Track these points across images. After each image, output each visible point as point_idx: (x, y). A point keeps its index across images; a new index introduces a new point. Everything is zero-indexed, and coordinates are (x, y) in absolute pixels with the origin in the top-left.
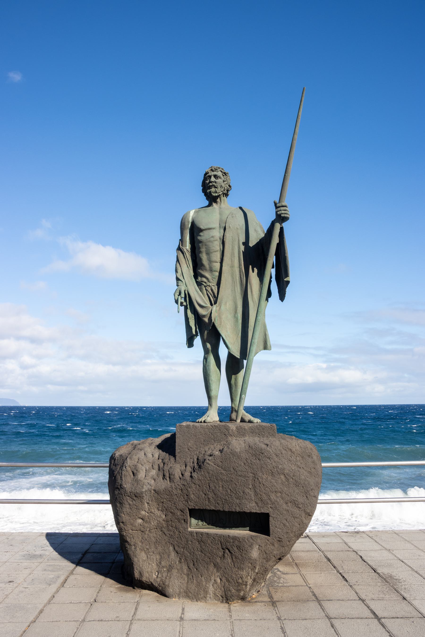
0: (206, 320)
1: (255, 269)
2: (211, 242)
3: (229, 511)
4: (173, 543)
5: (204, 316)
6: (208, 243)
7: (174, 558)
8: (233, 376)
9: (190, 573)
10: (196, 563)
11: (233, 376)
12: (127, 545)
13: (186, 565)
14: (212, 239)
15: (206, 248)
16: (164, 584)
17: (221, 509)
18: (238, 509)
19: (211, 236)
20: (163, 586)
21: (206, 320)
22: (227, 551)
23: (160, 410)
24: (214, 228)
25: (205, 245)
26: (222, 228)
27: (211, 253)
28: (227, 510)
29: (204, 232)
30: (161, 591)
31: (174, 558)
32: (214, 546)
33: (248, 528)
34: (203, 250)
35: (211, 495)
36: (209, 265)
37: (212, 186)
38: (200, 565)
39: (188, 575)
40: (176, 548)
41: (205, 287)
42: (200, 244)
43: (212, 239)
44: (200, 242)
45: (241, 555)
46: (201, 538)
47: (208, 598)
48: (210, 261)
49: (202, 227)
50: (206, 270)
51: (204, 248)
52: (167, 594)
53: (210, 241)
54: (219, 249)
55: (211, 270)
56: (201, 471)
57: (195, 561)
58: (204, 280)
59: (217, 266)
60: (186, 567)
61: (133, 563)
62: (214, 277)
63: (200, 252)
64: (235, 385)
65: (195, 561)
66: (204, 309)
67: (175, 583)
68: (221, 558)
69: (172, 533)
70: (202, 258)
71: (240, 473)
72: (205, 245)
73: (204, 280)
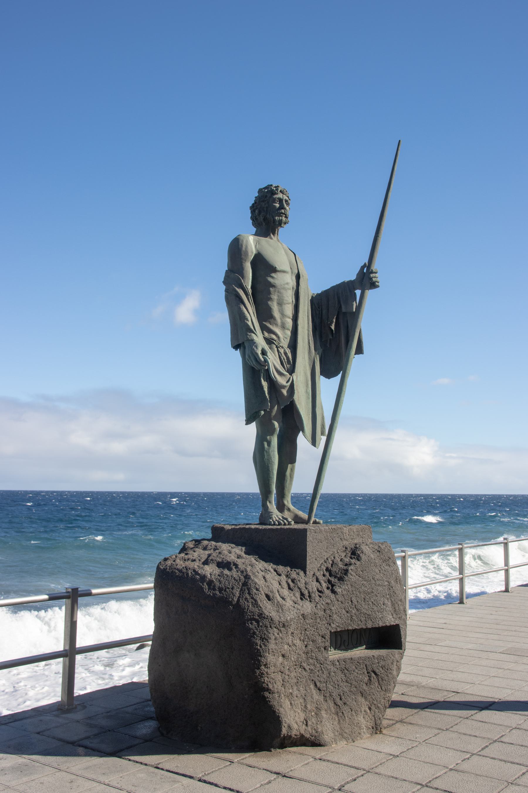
0: (285, 392)
2: (284, 289)
3: (372, 628)
4: (314, 679)
5: (284, 387)
6: (282, 291)
7: (317, 697)
8: (289, 465)
9: (338, 710)
10: (343, 697)
11: (289, 465)
12: (266, 694)
13: (332, 702)
14: (286, 286)
15: (278, 296)
16: (317, 732)
17: (364, 627)
18: (381, 624)
20: (316, 734)
21: (285, 392)
22: (373, 675)
23: (37, 505)
25: (278, 292)
27: (285, 304)
28: (369, 626)
29: (278, 273)
30: (314, 743)
31: (317, 697)
32: (359, 672)
33: (365, 646)
34: (275, 297)
35: (354, 612)
36: (281, 319)
37: (284, 214)
38: (348, 697)
39: (337, 714)
40: (318, 684)
41: (277, 347)
42: (271, 289)
43: (286, 286)
44: (273, 286)
45: (387, 676)
46: (344, 667)
47: (362, 734)
48: (283, 315)
49: (278, 268)
50: (277, 325)
52: (322, 742)
55: (283, 327)
56: (344, 584)
57: (342, 694)
58: (274, 337)
59: (289, 323)
60: (333, 705)
61: (279, 717)
62: (286, 336)
64: (291, 477)
65: (342, 694)
67: (328, 728)
68: (367, 684)
69: (312, 667)
70: (272, 307)
71: (378, 582)
72: (278, 292)
73: (274, 337)
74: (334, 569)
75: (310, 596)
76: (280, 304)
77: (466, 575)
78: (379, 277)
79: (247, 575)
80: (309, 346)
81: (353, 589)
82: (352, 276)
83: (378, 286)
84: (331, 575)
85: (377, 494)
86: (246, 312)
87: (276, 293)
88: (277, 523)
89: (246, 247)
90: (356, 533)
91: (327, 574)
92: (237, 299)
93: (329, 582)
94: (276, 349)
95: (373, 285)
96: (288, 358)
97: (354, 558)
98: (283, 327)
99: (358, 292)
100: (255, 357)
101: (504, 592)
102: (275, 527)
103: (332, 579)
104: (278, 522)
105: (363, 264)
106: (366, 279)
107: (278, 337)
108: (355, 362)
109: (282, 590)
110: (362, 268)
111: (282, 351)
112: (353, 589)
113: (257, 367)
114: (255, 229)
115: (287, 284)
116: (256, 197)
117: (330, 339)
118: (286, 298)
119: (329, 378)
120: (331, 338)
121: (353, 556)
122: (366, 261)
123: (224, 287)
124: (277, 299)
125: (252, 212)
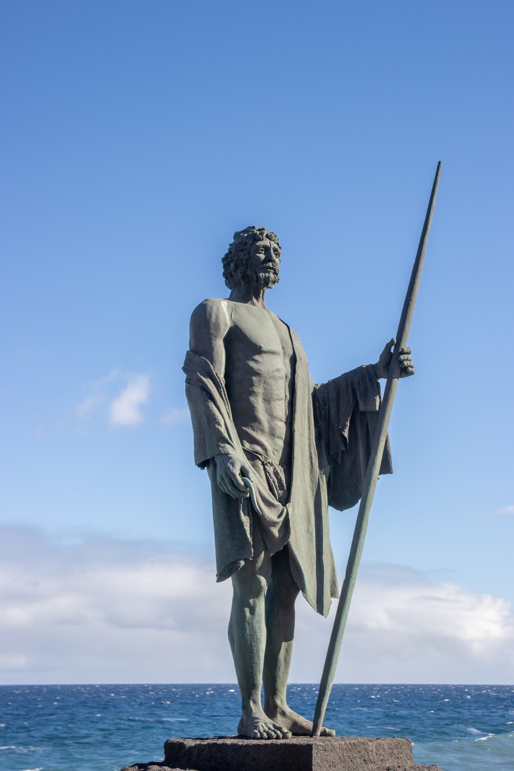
0: (275, 531)
1: (244, 441)
5: (274, 524)
6: (270, 381)
14: (277, 374)
15: (265, 389)
19: (275, 368)
21: (275, 531)
24: (273, 353)
25: (265, 382)
26: (288, 356)
27: (274, 400)
34: (259, 390)
36: (269, 422)
41: (263, 464)
42: (254, 378)
43: (277, 374)
44: (257, 374)
50: (262, 431)
51: (261, 387)
53: (273, 377)
54: (283, 395)
55: (272, 434)
58: (258, 449)
59: (281, 428)
62: (276, 448)
63: (253, 393)
64: (285, 661)
66: (273, 509)
70: (256, 405)
72: (265, 382)
73: (258, 449)
76: (267, 400)
80: (312, 462)
82: (375, 360)
83: (412, 373)
86: (217, 413)
87: (262, 384)
90: (388, 751)
92: (204, 392)
94: (262, 467)
95: (405, 372)
96: (280, 481)
98: (272, 434)
99: (383, 382)
100: (230, 479)
104: (268, 733)
105: (388, 341)
106: (394, 362)
107: (265, 450)
108: (380, 485)
110: (388, 346)
111: (270, 469)
113: (234, 494)
115: (278, 370)
116: (230, 245)
117: (343, 452)
119: (341, 511)
120: (344, 449)
124: (263, 393)
125: (224, 266)
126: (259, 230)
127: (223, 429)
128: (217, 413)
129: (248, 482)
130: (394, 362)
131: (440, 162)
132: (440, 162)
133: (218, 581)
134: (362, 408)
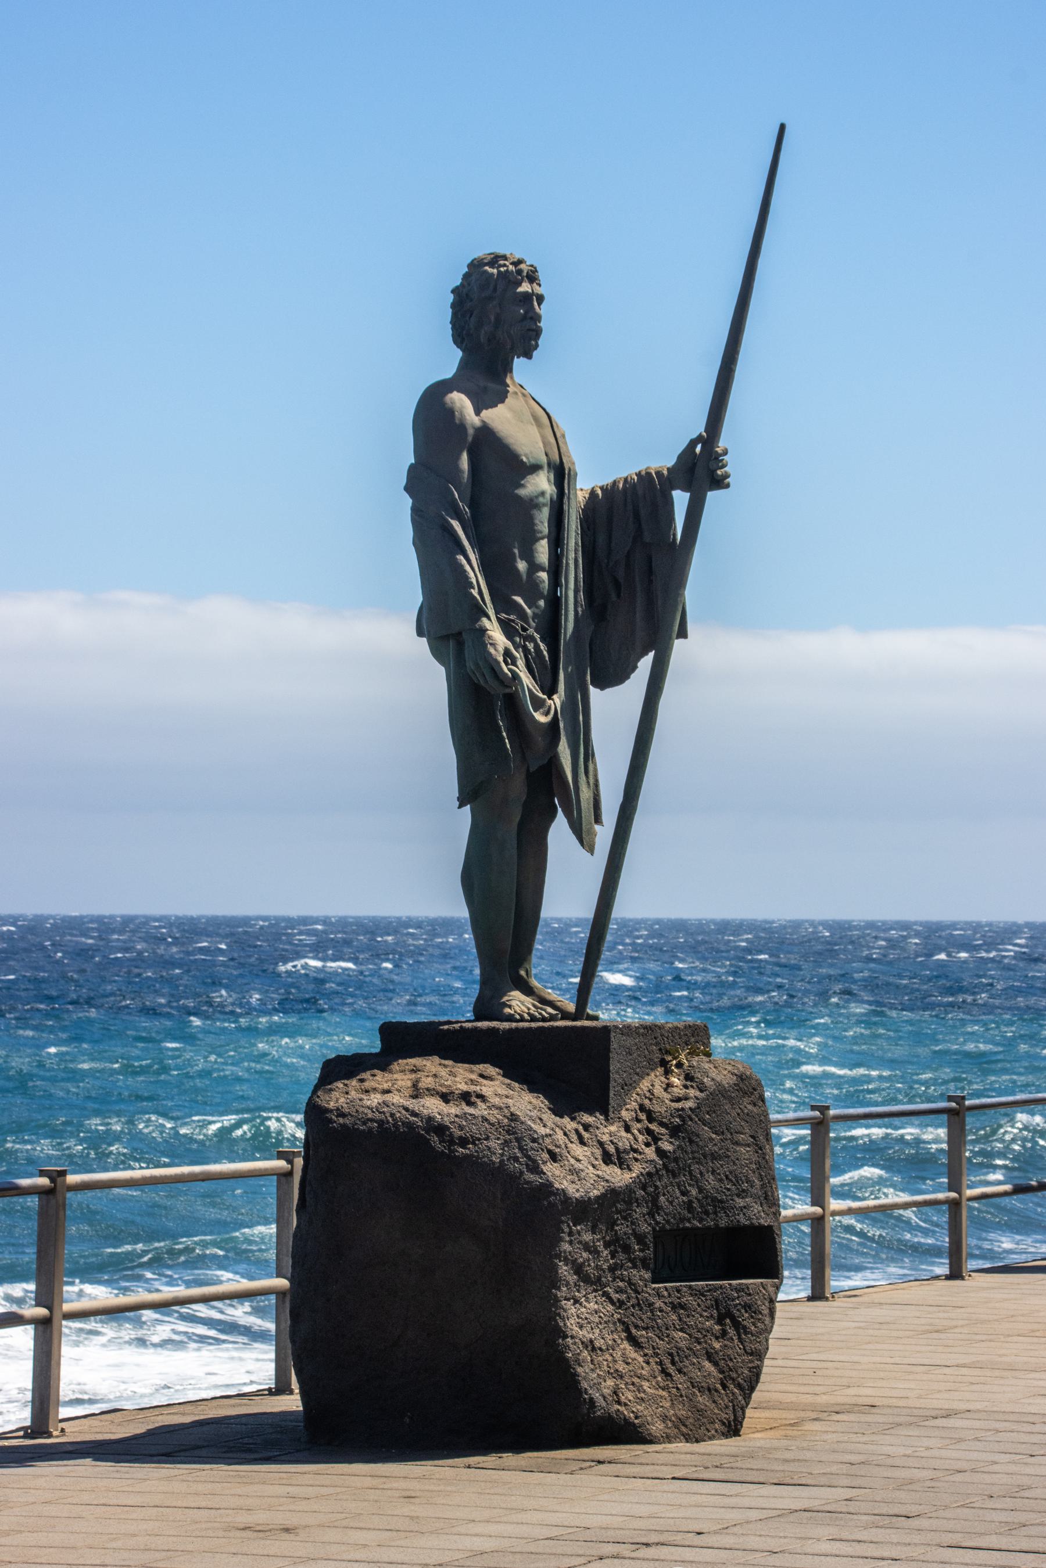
14: (541, 499)
43: (541, 499)
74: (657, 1108)
75: (619, 1158)
77: (67, 1307)
78: (733, 465)
79: (512, 1114)
81: (695, 1148)
82: (664, 459)
83: (728, 486)
84: (650, 1119)
85: (217, 917)
86: (468, 568)
88: (526, 1016)
89: (461, 413)
90: (684, 1039)
91: (643, 1117)
93: (649, 1132)
95: (719, 483)
97: (692, 1086)
99: (681, 499)
100: (493, 669)
101: (271, 1392)
102: (521, 1025)
103: (653, 1127)
104: (529, 1014)
105: (694, 436)
106: (702, 467)
109: (570, 1145)
110: (693, 443)
112: (695, 1148)
114: (459, 354)
115: (543, 494)
118: (539, 527)
121: (689, 1083)
122: (699, 428)
123: (409, 501)
126: (514, 264)
127: (475, 592)
128: (468, 568)
129: (518, 675)
130: (702, 467)
131: (782, 127)
132: (782, 127)
133: (459, 807)
134: (647, 538)
